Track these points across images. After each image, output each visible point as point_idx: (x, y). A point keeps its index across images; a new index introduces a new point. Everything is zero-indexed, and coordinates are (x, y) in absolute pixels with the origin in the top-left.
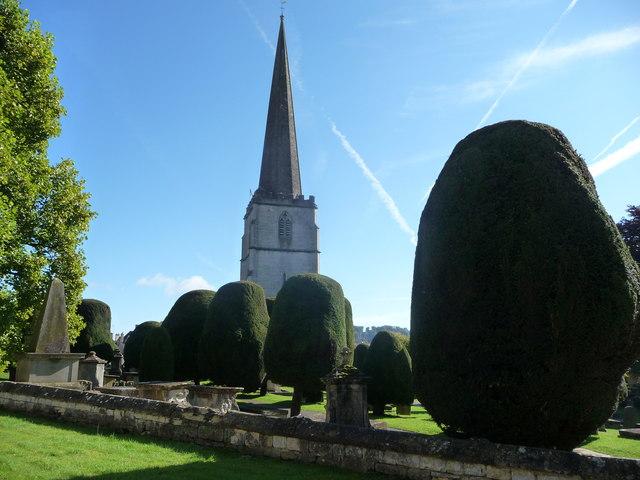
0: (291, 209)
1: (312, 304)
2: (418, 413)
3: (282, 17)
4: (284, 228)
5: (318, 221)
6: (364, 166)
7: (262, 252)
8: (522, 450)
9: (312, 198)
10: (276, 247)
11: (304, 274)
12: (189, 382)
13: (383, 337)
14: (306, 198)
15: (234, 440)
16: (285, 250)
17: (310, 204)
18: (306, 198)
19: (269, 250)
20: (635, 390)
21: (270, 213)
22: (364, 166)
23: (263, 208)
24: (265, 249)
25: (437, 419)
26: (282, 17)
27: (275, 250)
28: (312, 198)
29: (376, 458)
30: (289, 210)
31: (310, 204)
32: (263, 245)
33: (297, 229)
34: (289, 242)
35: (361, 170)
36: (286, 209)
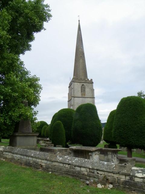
1: (90, 110)
3: (79, 21)
4: (83, 89)
5: (94, 88)
6: (103, 136)
9: (92, 80)
11: (91, 103)
12: (3, 146)
13: (43, 124)
14: (90, 80)
15: (61, 158)
18: (90, 80)
20: (0, 104)
22: (103, 136)
23: (76, 83)
26: (79, 21)
28: (92, 80)
33: (87, 90)
34: (85, 95)
35: (102, 136)
36: (83, 84)
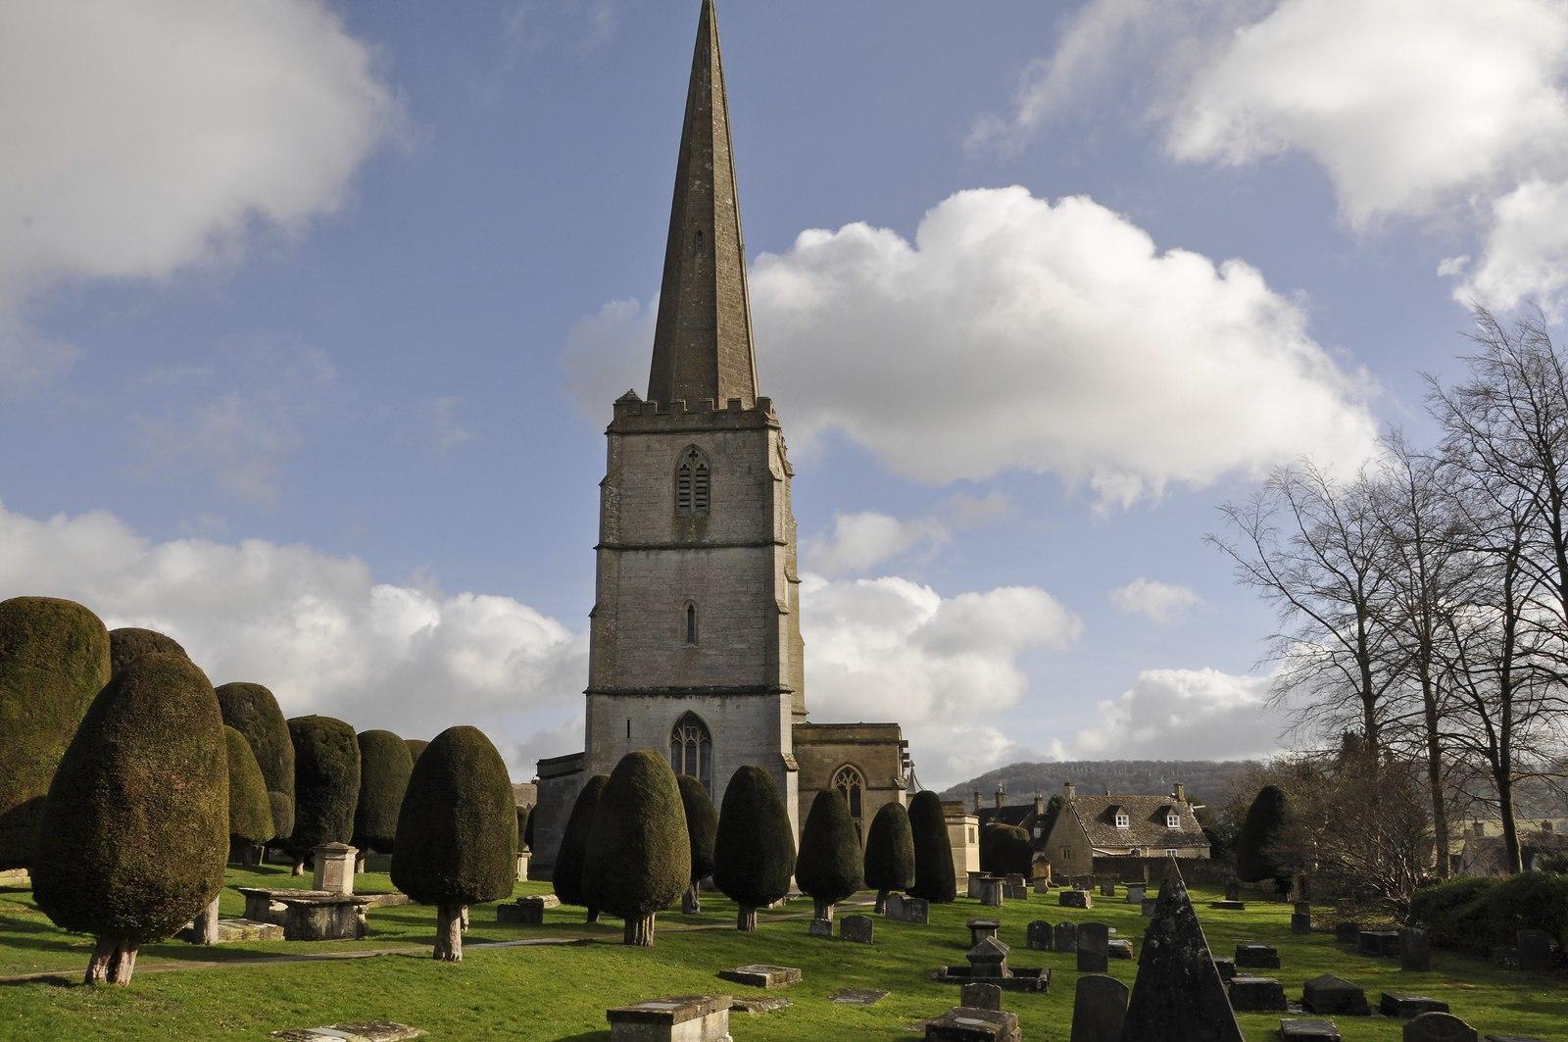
0: (706, 437)
2: (1557, 597)
4: (693, 484)
7: (631, 555)
8: (562, 836)
10: (668, 538)
16: (689, 547)
17: (758, 420)
19: (647, 548)
21: (661, 456)
23: (637, 441)
24: (636, 548)
25: (405, 893)
27: (663, 547)
29: (1283, 662)
30: (705, 442)
31: (905, 744)
32: (633, 537)
34: (702, 527)
36: (693, 439)
